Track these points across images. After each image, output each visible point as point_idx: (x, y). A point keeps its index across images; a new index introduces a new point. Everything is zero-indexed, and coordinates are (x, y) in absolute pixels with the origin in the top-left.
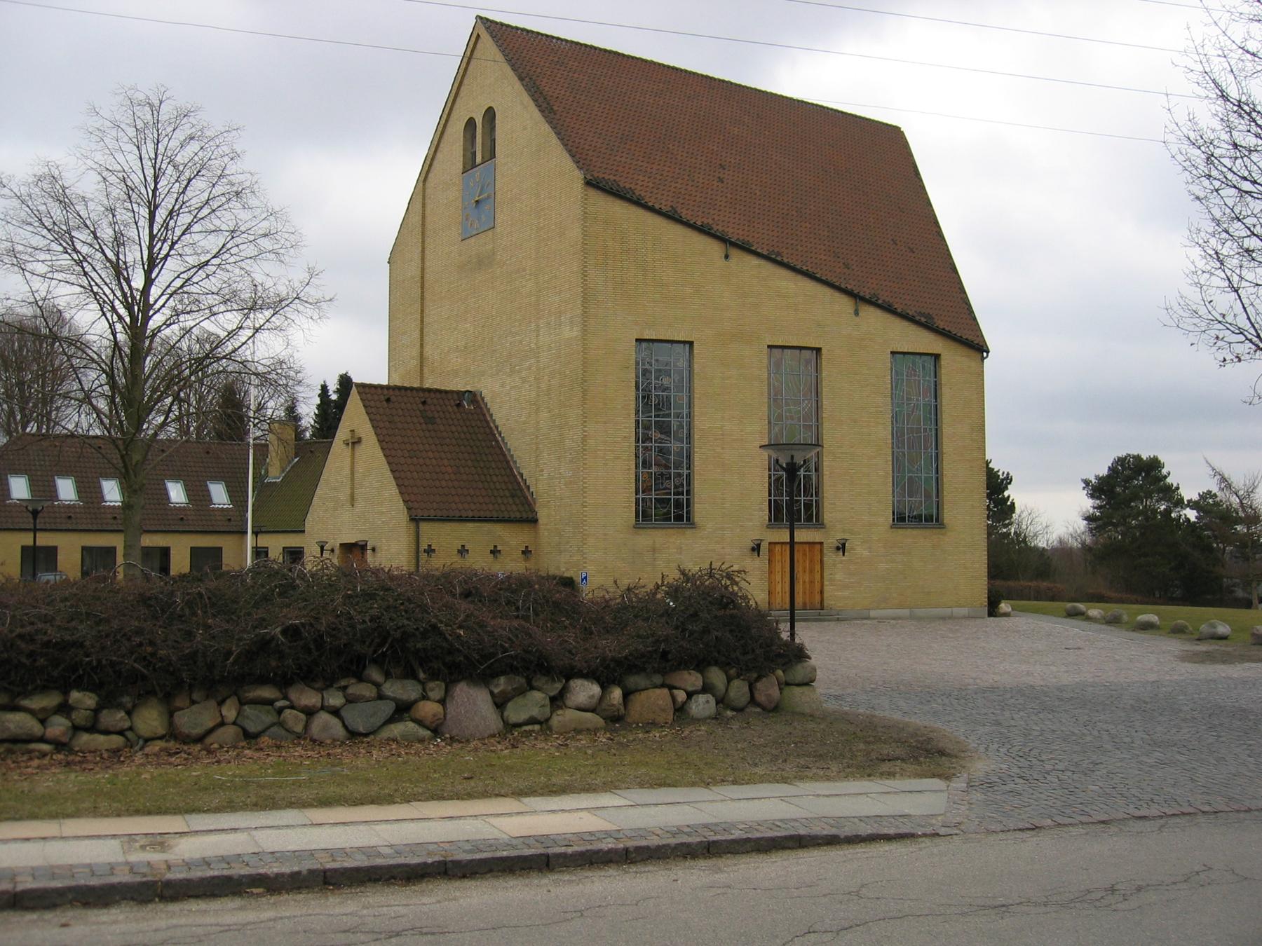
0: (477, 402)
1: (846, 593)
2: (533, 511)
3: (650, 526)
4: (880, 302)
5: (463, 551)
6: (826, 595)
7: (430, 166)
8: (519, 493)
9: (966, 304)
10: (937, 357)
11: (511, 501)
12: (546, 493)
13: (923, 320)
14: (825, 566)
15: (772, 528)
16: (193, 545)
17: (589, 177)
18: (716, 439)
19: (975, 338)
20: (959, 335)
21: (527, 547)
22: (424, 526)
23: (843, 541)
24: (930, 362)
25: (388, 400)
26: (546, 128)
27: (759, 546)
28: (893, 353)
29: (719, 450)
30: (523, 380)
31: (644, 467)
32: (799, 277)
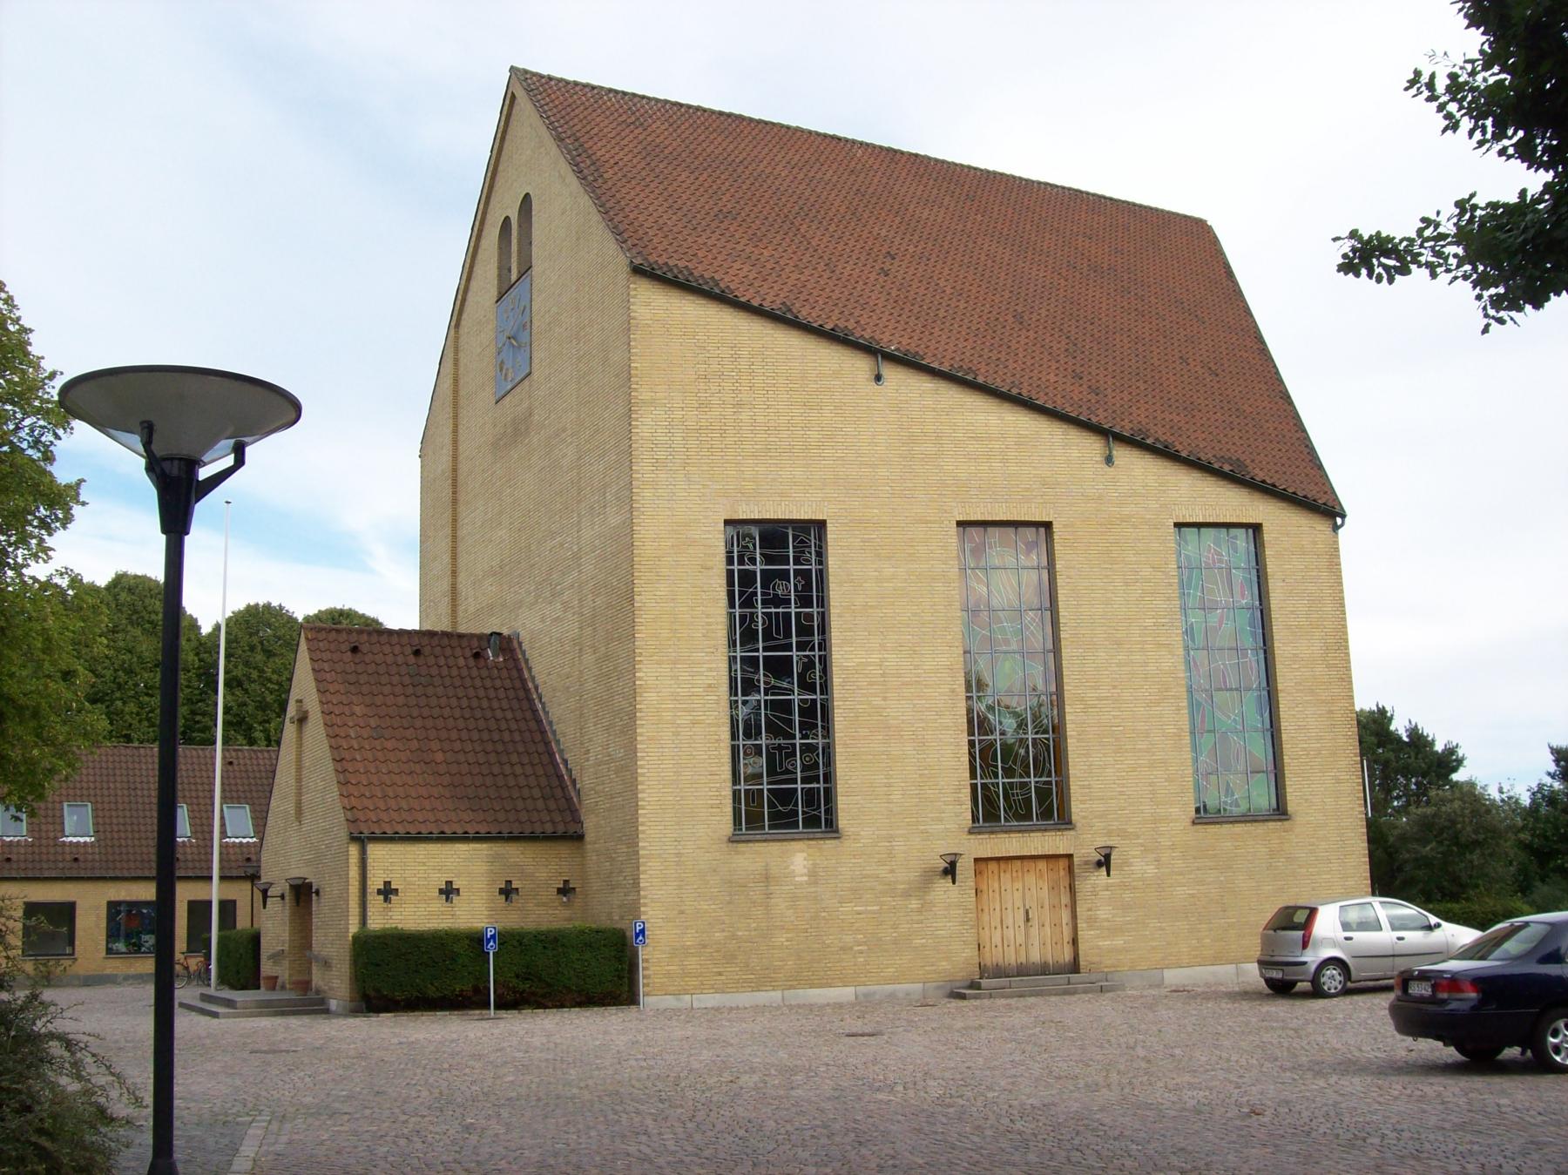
0: (512, 651)
1: (1119, 942)
2: (578, 821)
3: (796, 836)
4: (1149, 441)
5: (449, 891)
6: (1082, 947)
7: (464, 300)
8: (558, 792)
9: (1307, 446)
10: (1256, 528)
11: (540, 804)
12: (593, 789)
13: (1227, 468)
14: (1079, 896)
15: (980, 833)
16: (192, 898)
17: (638, 261)
18: (871, 684)
19: (1319, 495)
20: (1290, 490)
21: (566, 882)
22: (376, 851)
23: (952, 858)
24: (1242, 539)
25: (355, 650)
26: (585, 201)
27: (953, 865)
28: (1178, 525)
29: (878, 701)
30: (566, 606)
31: (748, 735)
32: (1006, 406)
